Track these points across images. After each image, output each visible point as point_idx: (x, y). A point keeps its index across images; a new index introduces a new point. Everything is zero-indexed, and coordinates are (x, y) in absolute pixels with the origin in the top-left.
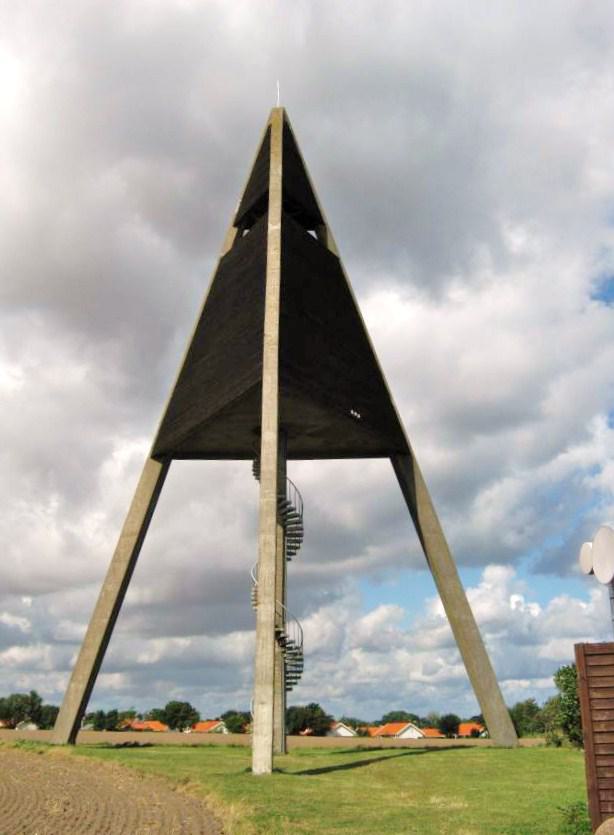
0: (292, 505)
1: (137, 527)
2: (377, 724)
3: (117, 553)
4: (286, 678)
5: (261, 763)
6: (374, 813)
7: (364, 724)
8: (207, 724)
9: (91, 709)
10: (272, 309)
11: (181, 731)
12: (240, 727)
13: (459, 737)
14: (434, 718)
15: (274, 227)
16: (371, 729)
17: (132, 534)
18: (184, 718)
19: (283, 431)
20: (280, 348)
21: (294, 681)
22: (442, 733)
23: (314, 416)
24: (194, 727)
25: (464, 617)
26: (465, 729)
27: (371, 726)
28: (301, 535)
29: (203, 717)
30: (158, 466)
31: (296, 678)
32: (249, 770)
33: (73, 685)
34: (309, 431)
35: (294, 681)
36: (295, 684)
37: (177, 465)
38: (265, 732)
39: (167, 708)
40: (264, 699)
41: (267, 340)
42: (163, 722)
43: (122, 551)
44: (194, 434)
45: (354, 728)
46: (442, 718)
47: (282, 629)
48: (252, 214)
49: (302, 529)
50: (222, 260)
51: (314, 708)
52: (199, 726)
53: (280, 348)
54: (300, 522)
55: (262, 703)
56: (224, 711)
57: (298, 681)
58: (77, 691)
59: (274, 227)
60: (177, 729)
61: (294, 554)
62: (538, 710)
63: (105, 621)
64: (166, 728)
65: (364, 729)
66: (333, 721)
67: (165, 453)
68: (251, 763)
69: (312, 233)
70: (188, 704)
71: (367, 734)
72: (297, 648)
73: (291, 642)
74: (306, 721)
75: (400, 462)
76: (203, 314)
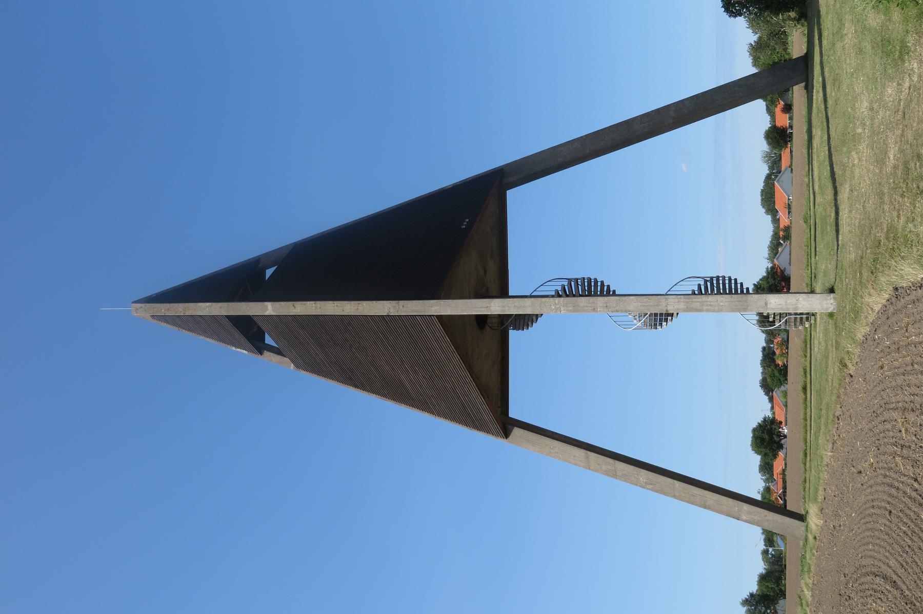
0: (559, 288)
1: (580, 453)
2: (776, 221)
3: (607, 473)
4: (736, 293)
5: (820, 304)
6: (869, 251)
7: (776, 236)
8: (777, 409)
10: (361, 308)
11: (785, 437)
12: (780, 371)
13: (791, 127)
14: (767, 157)
16: (782, 226)
17: (587, 458)
18: (771, 432)
19: (482, 293)
21: (739, 286)
22: (786, 144)
23: (468, 265)
24: (781, 423)
25: (672, 113)
26: (783, 120)
27: (779, 226)
28: (590, 280)
29: (769, 414)
30: (517, 432)
32: (831, 315)
33: (744, 518)
35: (739, 286)
36: (742, 284)
37: (513, 414)
38: (794, 301)
39: (758, 453)
40: (762, 303)
41: (393, 312)
42: (775, 456)
44: (484, 391)
45: (779, 244)
46: (769, 144)
48: (251, 333)
50: (298, 366)
52: (780, 417)
55: (766, 304)
56: (761, 392)
57: (739, 282)
58: (750, 513)
59: (270, 309)
60: (783, 442)
61: (608, 287)
62: (760, 38)
63: (677, 484)
64: (781, 454)
65: (781, 233)
66: (772, 268)
67: (505, 425)
68: (825, 314)
69: (269, 272)
70: (754, 430)
71: (787, 229)
72: (706, 282)
73: (699, 286)
74: (776, 281)
75: (511, 179)
76: (356, 386)
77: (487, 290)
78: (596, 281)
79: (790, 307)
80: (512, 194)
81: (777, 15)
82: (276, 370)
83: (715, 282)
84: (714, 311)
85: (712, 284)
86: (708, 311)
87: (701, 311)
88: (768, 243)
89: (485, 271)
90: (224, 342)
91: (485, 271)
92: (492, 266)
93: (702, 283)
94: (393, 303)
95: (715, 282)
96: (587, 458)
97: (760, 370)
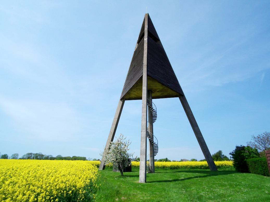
0: (154, 109)
9: (147, 160)
15: (146, 39)
20: (154, 73)
21: (156, 153)
23: (157, 86)
25: (198, 130)
28: (156, 116)
31: (157, 153)
34: (158, 90)
35: (156, 153)
37: (126, 102)
43: (151, 127)
47: (152, 140)
49: (157, 115)
51: (237, 147)
53: (154, 73)
54: (156, 113)
59: (146, 39)
67: (123, 99)
72: (156, 145)
73: (155, 143)
77: (154, 93)
78: (156, 118)
79: (141, 168)
80: (178, 98)
81: (248, 165)
82: (134, 46)
83: (157, 147)
84: (141, 145)
85: (156, 146)
86: (141, 143)
87: (141, 141)
88: (65, 156)
89: (158, 92)
90: (144, 42)
91: (158, 92)
92: (159, 94)
93: (156, 144)
94: (146, 65)
95: (157, 147)
96: (116, 119)
97: (64, 157)
